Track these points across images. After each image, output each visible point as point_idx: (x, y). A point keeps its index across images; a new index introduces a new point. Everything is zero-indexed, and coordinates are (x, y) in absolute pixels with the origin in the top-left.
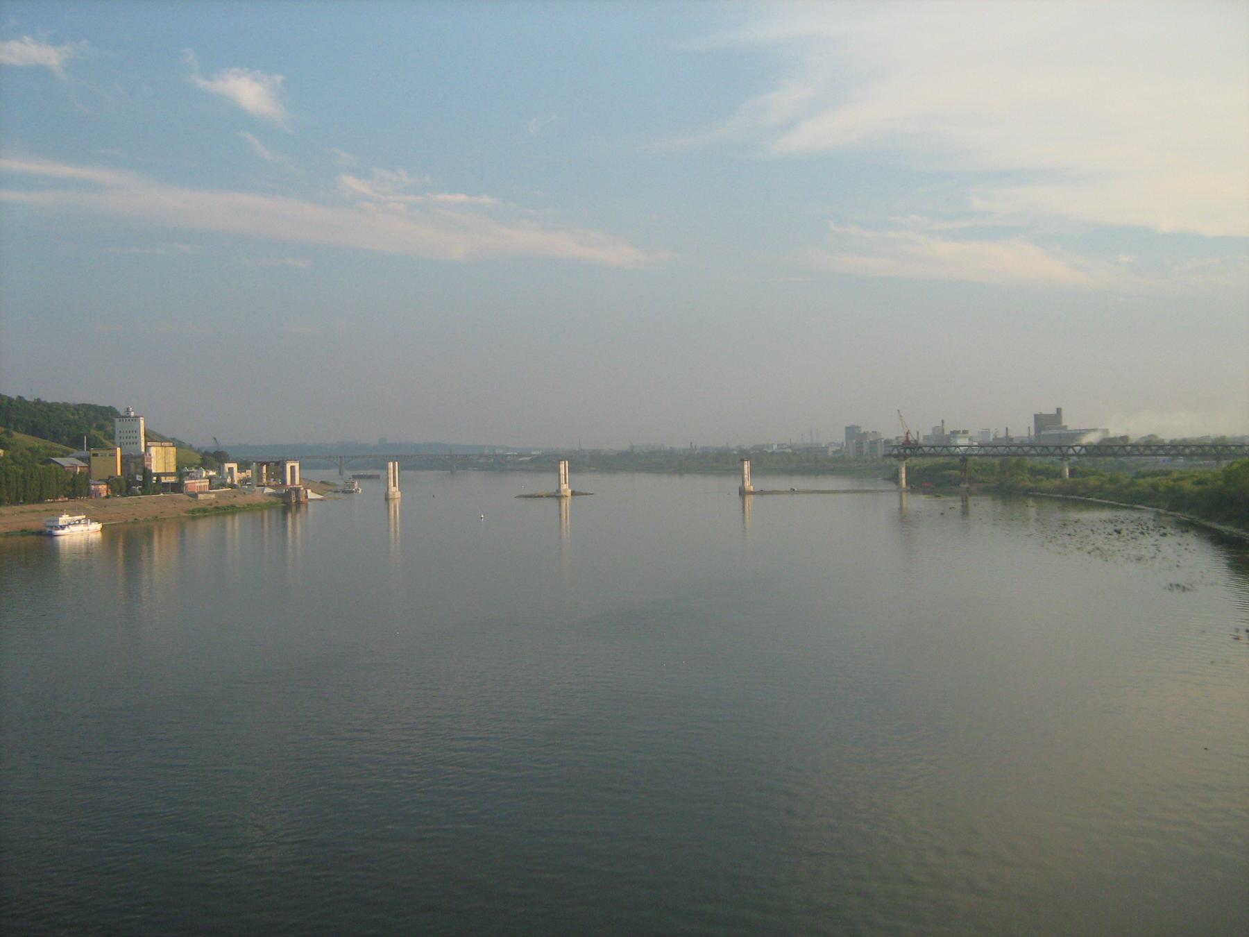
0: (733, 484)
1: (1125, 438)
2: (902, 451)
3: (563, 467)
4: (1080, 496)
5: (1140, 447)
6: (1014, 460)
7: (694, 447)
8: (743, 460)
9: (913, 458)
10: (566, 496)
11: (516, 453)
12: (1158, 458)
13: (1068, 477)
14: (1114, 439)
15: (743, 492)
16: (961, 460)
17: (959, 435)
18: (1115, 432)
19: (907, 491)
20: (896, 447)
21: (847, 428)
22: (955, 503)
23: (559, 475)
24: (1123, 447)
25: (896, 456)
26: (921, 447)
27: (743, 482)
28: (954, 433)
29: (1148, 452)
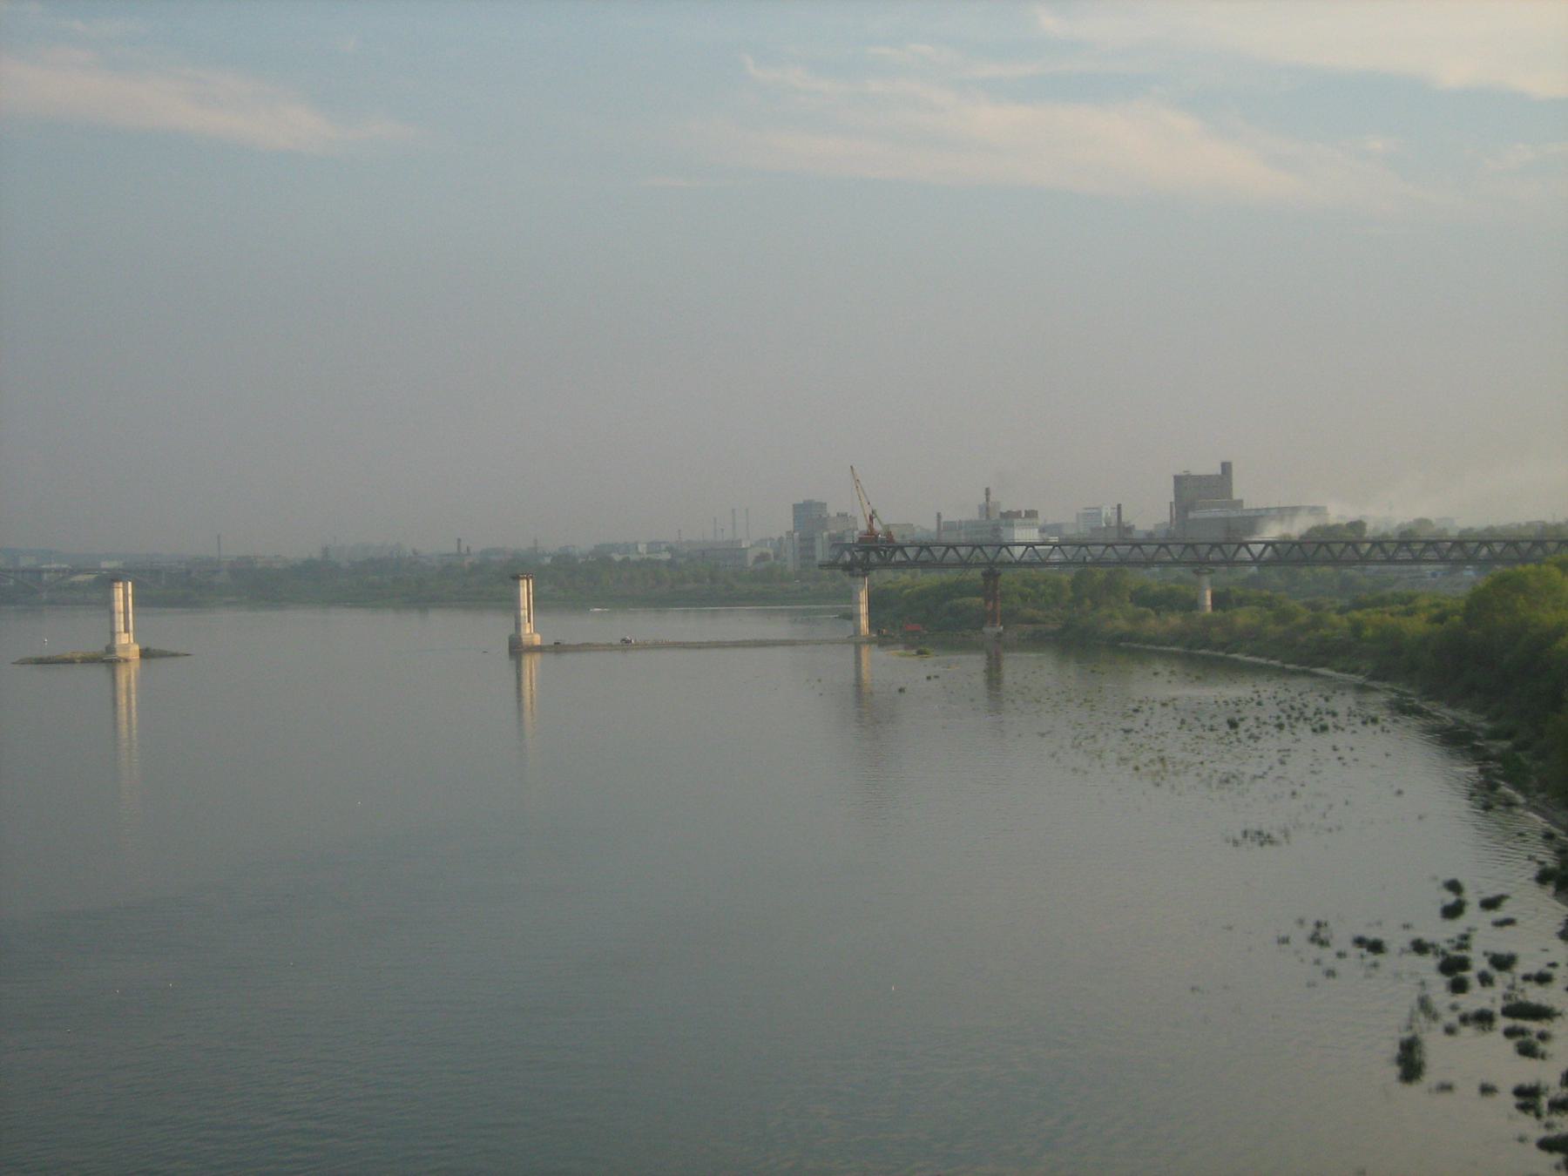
0: (490, 629)
1: (1357, 526)
2: (859, 555)
3: (122, 595)
4: (1216, 650)
5: (1386, 546)
6: (1101, 574)
7: (464, 550)
8: (517, 578)
9: (919, 571)
10: (127, 661)
11: (65, 566)
12: (1423, 567)
13: (1209, 610)
14: (1337, 527)
15: (517, 649)
16: (984, 574)
17: (1016, 521)
18: (1338, 513)
19: (870, 641)
20: (848, 547)
21: (796, 507)
22: (972, 665)
23: (112, 612)
24: (1353, 544)
25: (848, 567)
26: (901, 548)
27: (518, 626)
28: (1009, 516)
29: (1403, 555)
